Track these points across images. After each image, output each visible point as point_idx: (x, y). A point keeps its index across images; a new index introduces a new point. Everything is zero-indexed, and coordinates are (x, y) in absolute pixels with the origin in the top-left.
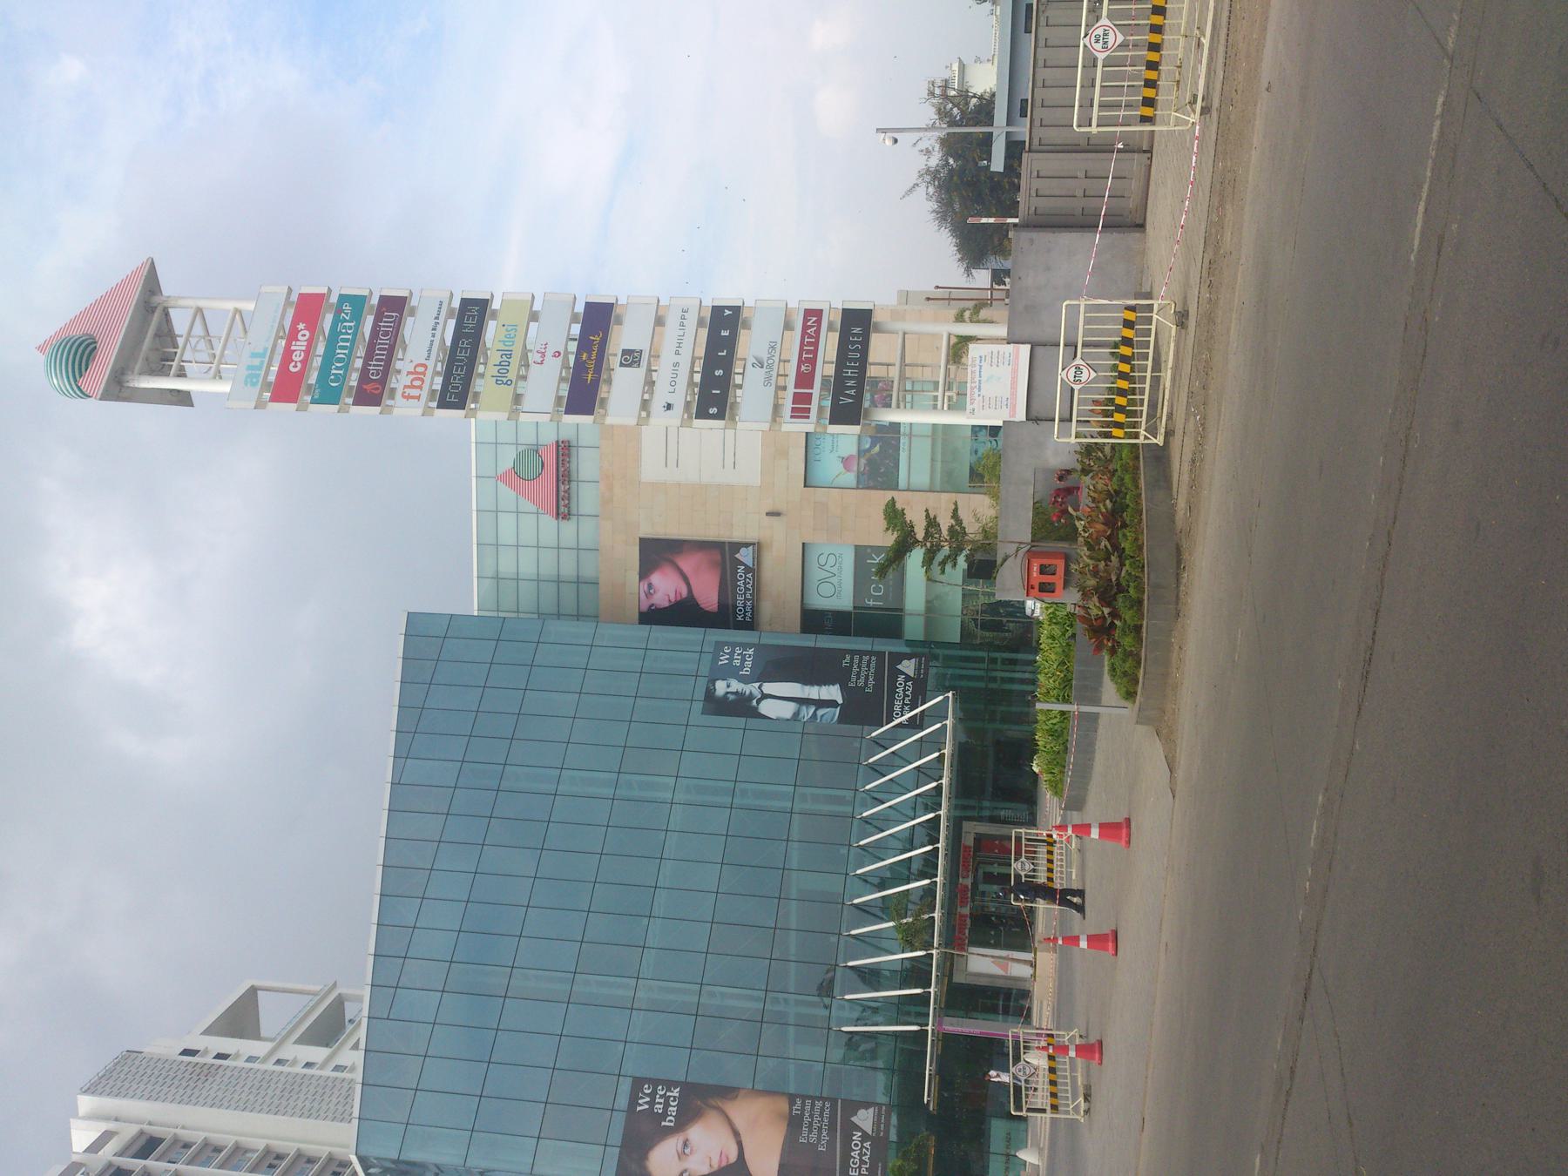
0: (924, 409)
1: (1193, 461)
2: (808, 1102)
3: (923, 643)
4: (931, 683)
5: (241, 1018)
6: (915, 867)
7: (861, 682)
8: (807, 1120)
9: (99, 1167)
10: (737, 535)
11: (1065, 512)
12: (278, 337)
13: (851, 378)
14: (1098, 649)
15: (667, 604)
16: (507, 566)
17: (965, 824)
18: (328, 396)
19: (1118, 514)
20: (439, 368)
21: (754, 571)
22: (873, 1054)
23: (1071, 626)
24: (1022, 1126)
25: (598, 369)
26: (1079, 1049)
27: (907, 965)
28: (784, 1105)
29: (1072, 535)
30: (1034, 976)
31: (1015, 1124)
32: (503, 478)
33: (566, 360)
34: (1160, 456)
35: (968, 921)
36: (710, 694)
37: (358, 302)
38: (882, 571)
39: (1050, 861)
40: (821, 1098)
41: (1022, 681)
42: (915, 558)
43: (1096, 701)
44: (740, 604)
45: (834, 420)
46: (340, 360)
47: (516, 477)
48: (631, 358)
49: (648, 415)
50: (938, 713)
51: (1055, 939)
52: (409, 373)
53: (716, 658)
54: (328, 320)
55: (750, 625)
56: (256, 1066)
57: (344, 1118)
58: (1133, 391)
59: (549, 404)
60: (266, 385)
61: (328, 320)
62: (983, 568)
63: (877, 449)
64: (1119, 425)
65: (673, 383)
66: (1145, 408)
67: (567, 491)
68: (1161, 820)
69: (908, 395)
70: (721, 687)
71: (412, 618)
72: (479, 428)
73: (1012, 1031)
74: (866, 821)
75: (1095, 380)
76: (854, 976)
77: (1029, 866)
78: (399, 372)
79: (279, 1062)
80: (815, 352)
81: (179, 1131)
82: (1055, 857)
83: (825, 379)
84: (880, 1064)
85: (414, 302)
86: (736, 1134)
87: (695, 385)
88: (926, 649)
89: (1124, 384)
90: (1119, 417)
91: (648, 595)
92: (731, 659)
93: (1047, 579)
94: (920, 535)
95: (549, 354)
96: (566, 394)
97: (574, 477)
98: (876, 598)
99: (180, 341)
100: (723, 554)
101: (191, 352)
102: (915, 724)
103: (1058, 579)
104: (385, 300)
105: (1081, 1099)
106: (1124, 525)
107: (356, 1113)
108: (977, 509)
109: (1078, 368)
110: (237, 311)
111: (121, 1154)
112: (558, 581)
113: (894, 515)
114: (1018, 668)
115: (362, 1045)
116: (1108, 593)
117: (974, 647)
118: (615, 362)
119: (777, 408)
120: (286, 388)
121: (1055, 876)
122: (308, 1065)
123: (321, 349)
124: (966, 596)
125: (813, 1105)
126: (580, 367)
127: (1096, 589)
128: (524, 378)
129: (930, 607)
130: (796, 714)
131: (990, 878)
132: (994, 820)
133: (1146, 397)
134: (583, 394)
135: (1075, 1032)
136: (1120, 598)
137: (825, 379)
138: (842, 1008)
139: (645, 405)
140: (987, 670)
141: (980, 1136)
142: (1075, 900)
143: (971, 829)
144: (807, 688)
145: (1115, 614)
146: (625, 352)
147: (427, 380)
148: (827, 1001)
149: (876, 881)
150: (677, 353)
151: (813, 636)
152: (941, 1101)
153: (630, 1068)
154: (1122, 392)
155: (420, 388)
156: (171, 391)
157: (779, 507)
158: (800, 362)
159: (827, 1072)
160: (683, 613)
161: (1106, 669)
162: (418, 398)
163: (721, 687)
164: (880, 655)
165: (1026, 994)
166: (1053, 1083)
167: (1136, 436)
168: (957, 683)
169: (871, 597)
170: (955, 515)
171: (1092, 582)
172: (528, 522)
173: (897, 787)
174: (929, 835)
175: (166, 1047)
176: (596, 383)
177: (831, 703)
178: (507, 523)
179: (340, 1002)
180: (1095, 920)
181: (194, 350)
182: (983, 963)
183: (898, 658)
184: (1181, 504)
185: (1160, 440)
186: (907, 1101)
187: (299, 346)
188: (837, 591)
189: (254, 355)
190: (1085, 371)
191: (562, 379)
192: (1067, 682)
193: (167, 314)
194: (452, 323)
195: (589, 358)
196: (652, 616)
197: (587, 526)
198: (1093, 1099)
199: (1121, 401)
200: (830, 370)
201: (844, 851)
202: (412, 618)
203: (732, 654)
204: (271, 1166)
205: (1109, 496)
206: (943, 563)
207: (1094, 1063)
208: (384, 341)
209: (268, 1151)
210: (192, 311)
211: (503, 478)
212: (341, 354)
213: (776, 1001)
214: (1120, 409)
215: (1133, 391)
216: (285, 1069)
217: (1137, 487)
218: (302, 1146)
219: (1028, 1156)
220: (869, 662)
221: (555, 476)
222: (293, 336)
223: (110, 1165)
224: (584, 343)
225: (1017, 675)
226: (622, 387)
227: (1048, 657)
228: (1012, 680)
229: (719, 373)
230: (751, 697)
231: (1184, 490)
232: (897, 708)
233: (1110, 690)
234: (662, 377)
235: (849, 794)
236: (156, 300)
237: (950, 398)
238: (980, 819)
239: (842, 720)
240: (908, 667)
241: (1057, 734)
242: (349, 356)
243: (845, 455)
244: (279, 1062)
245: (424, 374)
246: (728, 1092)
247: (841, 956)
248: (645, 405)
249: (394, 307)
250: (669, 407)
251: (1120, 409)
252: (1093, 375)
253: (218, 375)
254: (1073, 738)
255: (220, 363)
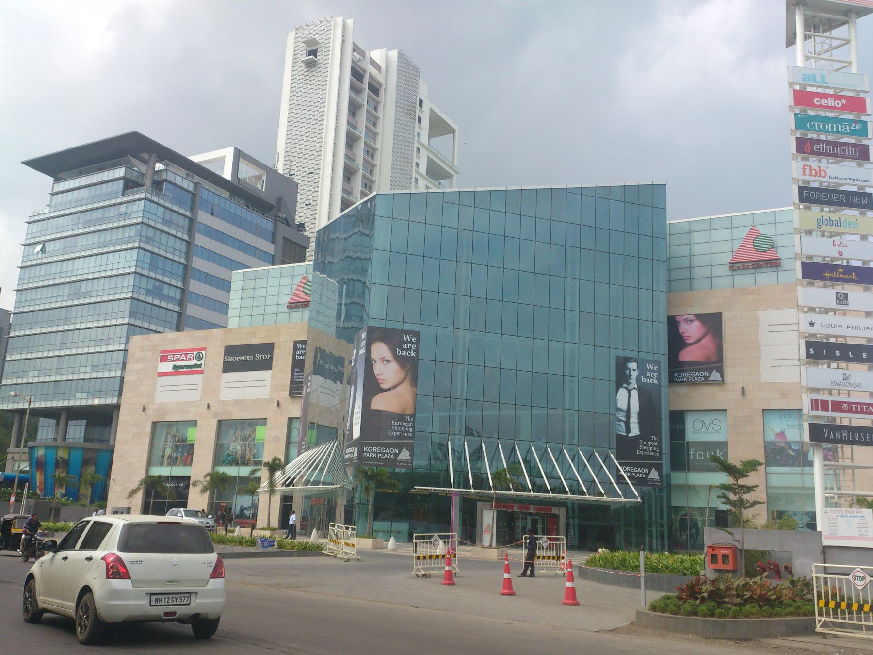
0: (824, 481)
1: (808, 650)
2: (411, 424)
3: (669, 485)
4: (644, 488)
5: (439, 127)
6: (537, 480)
7: (642, 447)
8: (403, 424)
9: (364, 67)
10: (727, 370)
11: (764, 570)
12: (835, 89)
13: (841, 435)
14: (681, 590)
15: (681, 331)
16: (697, 237)
17: (564, 509)
18: (800, 122)
19: (767, 603)
20: (824, 184)
21: (706, 381)
22: (437, 459)
23: (691, 573)
24: (406, 540)
25: (832, 279)
26: (449, 572)
27: (484, 476)
28: (409, 411)
29: (750, 574)
30: (483, 547)
31: (406, 536)
32: (753, 229)
33: (838, 259)
34: (808, 629)
35: (510, 510)
36: (628, 359)
37: (863, 132)
38: (714, 459)
39: (549, 558)
40: (414, 430)
41: (651, 543)
42: (723, 478)
43: (646, 588)
44: (684, 374)
45: (811, 426)
46: (824, 126)
47: (755, 236)
48: (842, 299)
49: (805, 312)
50: (627, 493)
51: (507, 560)
52: (820, 167)
53: (650, 362)
54: (850, 116)
55: (672, 380)
56: (416, 138)
57: (392, 186)
58: (851, 613)
59: (807, 251)
60: (804, 86)
61: (850, 116)
62: (722, 520)
63: (792, 453)
64: (827, 604)
65: (828, 325)
66: (840, 620)
67: (748, 267)
68: (581, 622)
69: (833, 471)
70: (633, 366)
71: (661, 189)
72: (792, 213)
73: (455, 535)
74: (561, 452)
75: (856, 589)
76: (477, 447)
77: (545, 545)
78: (820, 161)
79: (418, 149)
80: (856, 412)
81: (382, 104)
82: (551, 561)
83: (834, 419)
84: (432, 462)
85: (866, 165)
86: (394, 387)
87: (828, 339)
88: (665, 486)
89: (855, 607)
90: (832, 604)
91: (686, 320)
92: (650, 371)
93: (720, 558)
94: (742, 482)
95: (840, 249)
96: (815, 261)
97: (758, 271)
98: (694, 455)
99: (827, 34)
100: (715, 362)
101: (820, 41)
102: (620, 479)
103: (720, 566)
104: (866, 147)
105: (423, 573)
106: (761, 607)
107: (396, 192)
108: (758, 516)
109: (864, 578)
110: (850, 63)
111: (370, 76)
112: (690, 268)
113: (752, 465)
114: (659, 540)
115: (430, 191)
116: (716, 596)
117: (669, 515)
118: (839, 288)
119: (817, 390)
120: (802, 98)
121: (541, 561)
122: (417, 164)
123: (830, 114)
124: (701, 510)
125: (410, 427)
126: (833, 268)
127: (718, 589)
128: (823, 235)
129: (692, 488)
130: (620, 410)
131: (535, 522)
132: (568, 525)
133: (847, 621)
134: (815, 271)
135: (458, 570)
136: (713, 603)
137: (834, 419)
138: (460, 440)
139: (812, 309)
140: (656, 523)
141: (398, 516)
142: (529, 572)
143: (561, 512)
144: (636, 416)
145: (703, 600)
146: (846, 295)
147: (817, 178)
148: (463, 432)
149: (528, 458)
150: (848, 327)
151: (668, 418)
152: (415, 495)
153: (424, 331)
154: (849, 606)
155: (811, 175)
156: (795, 34)
157: (748, 395)
158: (849, 403)
159: (427, 434)
160: (676, 341)
161: (669, 594)
162: (804, 174)
163: (633, 366)
164: (660, 458)
165: (473, 542)
166: (431, 557)
167: (820, 615)
168: (646, 504)
169: (695, 451)
170: (755, 503)
171: (722, 586)
172: (727, 247)
173: (582, 469)
174: (556, 488)
175: (423, 91)
176: (823, 278)
177: (628, 430)
178: (726, 234)
179: (449, 176)
180: (519, 584)
181: (822, 43)
182: (488, 518)
183: (659, 468)
184: (778, 642)
185: (818, 629)
186: (414, 478)
187: (831, 102)
188: (696, 431)
189: (822, 77)
190: (862, 583)
191: (824, 258)
192: (655, 570)
193: (844, 24)
194: (855, 189)
195: (840, 273)
196: (673, 323)
197: (726, 282)
198: (424, 579)
199: (844, 605)
200: (846, 422)
201: (544, 439)
202: (661, 189)
203: (654, 371)
204: (368, 152)
205: (779, 598)
206: (724, 496)
207: (443, 580)
208: (840, 150)
209: (375, 150)
210: (847, 37)
211: (753, 229)
212: (829, 127)
213: (462, 405)
214: (838, 605)
215: (851, 613)
216: (415, 153)
217: (786, 615)
218: (378, 167)
219: (392, 543)
220: (655, 451)
221: (758, 259)
222: (837, 97)
223: (365, 71)
224: (848, 269)
225: (654, 541)
226: (822, 295)
227: (667, 559)
228: (651, 536)
229: (837, 353)
230: (629, 383)
231: (787, 644)
232: (628, 469)
233: (655, 596)
234: (830, 318)
235: (576, 441)
236: (853, 16)
237: (833, 498)
238: (567, 518)
239: (619, 437)
240: (654, 475)
241: (623, 564)
242: (827, 131)
243: (786, 433)
244: (418, 149)
245: (820, 176)
246: (414, 382)
247: (486, 439)
248: (812, 309)
249: (862, 154)
250: (812, 324)
251: (838, 605)
252: (860, 588)
253: (807, 58)
254: (623, 573)
255: (815, 58)
